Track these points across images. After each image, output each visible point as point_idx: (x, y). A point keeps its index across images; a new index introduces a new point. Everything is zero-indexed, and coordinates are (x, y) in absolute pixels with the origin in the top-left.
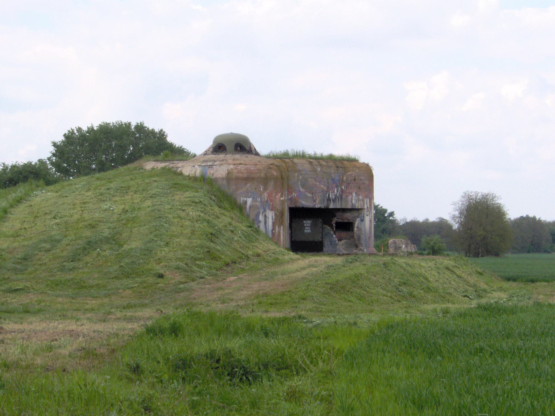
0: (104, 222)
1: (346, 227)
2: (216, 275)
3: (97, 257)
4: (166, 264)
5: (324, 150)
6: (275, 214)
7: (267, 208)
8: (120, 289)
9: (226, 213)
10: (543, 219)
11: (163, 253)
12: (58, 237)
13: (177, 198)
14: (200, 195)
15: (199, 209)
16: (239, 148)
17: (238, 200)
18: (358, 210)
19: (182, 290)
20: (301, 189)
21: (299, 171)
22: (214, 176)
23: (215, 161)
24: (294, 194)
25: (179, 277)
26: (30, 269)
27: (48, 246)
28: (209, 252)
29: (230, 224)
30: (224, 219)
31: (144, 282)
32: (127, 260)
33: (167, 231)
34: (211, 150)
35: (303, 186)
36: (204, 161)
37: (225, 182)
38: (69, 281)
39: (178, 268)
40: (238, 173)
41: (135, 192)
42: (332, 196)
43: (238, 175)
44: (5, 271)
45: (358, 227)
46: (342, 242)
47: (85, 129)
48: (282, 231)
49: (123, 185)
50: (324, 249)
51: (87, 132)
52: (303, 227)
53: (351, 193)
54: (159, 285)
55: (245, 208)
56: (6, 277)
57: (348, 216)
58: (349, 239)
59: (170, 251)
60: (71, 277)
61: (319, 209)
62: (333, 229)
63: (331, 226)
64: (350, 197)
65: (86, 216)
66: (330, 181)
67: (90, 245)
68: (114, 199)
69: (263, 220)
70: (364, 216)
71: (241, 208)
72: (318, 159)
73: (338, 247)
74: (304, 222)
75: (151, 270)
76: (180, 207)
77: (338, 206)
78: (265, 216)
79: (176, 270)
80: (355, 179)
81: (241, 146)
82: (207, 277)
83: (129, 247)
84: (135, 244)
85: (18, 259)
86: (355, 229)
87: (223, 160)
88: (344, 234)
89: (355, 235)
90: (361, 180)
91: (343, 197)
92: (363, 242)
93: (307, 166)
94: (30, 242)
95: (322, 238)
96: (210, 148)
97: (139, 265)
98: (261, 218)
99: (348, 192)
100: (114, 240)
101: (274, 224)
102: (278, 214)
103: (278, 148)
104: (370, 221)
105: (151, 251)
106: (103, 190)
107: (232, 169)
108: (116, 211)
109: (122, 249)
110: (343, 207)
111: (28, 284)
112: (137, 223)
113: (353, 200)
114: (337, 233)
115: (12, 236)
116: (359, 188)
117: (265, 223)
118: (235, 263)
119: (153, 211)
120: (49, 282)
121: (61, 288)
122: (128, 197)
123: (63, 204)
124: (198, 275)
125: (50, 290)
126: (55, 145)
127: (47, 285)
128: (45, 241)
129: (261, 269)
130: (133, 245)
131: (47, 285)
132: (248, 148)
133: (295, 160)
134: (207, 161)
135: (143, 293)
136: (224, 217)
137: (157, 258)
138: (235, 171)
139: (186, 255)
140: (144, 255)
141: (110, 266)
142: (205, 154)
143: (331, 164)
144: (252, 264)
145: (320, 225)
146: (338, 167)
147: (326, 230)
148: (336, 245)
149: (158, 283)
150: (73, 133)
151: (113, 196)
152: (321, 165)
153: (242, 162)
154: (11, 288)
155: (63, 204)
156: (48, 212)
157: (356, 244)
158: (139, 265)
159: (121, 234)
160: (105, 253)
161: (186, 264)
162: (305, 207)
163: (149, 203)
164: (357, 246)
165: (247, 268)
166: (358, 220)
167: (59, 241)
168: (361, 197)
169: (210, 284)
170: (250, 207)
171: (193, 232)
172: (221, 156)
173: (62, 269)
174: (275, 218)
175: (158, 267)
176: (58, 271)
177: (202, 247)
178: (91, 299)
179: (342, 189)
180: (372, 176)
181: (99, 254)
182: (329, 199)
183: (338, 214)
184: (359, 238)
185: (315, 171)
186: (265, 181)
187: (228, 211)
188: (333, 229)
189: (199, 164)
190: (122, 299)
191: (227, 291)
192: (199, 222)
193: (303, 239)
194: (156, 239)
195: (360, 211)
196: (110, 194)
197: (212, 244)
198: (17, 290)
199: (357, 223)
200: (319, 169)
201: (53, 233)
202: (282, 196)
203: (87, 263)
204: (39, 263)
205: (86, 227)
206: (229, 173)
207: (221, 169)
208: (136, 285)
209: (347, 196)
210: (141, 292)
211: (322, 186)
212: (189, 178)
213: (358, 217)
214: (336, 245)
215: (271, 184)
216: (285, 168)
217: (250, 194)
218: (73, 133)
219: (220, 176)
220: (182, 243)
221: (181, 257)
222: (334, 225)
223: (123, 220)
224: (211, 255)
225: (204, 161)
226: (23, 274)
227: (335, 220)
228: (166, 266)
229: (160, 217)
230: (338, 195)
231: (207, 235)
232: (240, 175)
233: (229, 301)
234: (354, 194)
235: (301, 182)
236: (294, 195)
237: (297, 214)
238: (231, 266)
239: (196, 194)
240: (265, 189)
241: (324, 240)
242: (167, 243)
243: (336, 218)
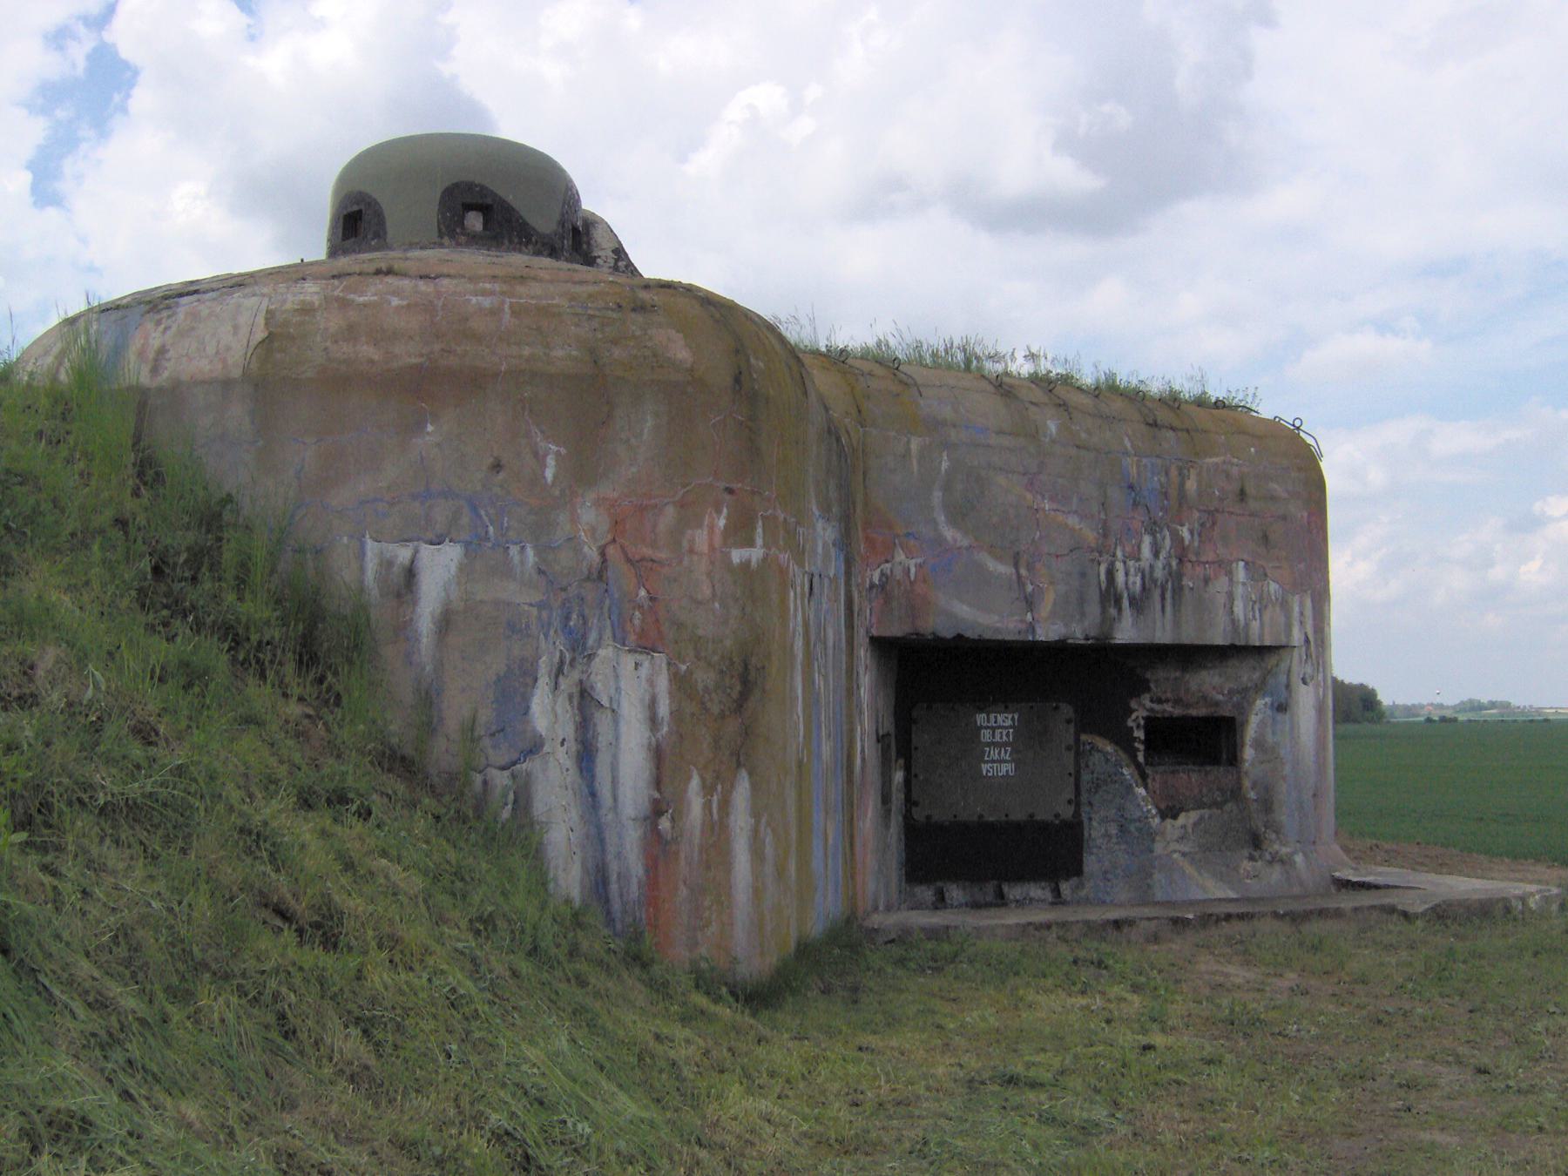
1: (1204, 741)
6: (681, 683)
18: (1262, 651)
20: (949, 533)
21: (934, 425)
24: (900, 556)
35: (959, 514)
37: (238, 414)
42: (1127, 579)
43: (345, 349)
45: (1259, 744)
46: (1182, 819)
48: (740, 820)
50: (1090, 863)
52: (971, 745)
53: (1224, 566)
55: (403, 630)
58: (1218, 805)
61: (1059, 651)
62: (1134, 758)
63: (1123, 740)
64: (1221, 584)
66: (1116, 494)
69: (567, 729)
70: (1288, 686)
72: (1054, 390)
73: (1159, 848)
74: (981, 718)
77: (1163, 634)
78: (585, 698)
80: (1242, 495)
86: (1248, 753)
88: (1189, 779)
89: (1247, 783)
90: (1273, 498)
91: (1187, 582)
92: (1283, 816)
95: (1077, 804)
98: (547, 712)
99: (1210, 556)
102: (704, 678)
104: (1320, 710)
107: (306, 310)
110: (1189, 636)
113: (1233, 604)
114: (1156, 777)
116: (1265, 537)
117: (586, 756)
132: (544, 223)
138: (333, 322)
143: (1118, 404)
145: (1067, 734)
148: (1151, 836)
162: (969, 634)
164: (1256, 842)
166: (1260, 703)
168: (1273, 587)
170: (446, 622)
174: (676, 715)
179: (1177, 539)
180: (1316, 485)
182: (1110, 596)
183: (1162, 678)
184: (1267, 805)
188: (1134, 758)
193: (971, 808)
195: (1271, 661)
200: (1052, 427)
202: (740, 531)
209: (1206, 581)
211: (1073, 521)
213: (1260, 688)
215: (640, 434)
219: (203, 366)
222: (1140, 734)
227: (1140, 710)
230: (1159, 573)
232: (367, 351)
234: (1240, 573)
235: (947, 488)
236: (904, 562)
237: (933, 676)
240: (582, 472)
241: (1085, 809)
243: (1146, 699)
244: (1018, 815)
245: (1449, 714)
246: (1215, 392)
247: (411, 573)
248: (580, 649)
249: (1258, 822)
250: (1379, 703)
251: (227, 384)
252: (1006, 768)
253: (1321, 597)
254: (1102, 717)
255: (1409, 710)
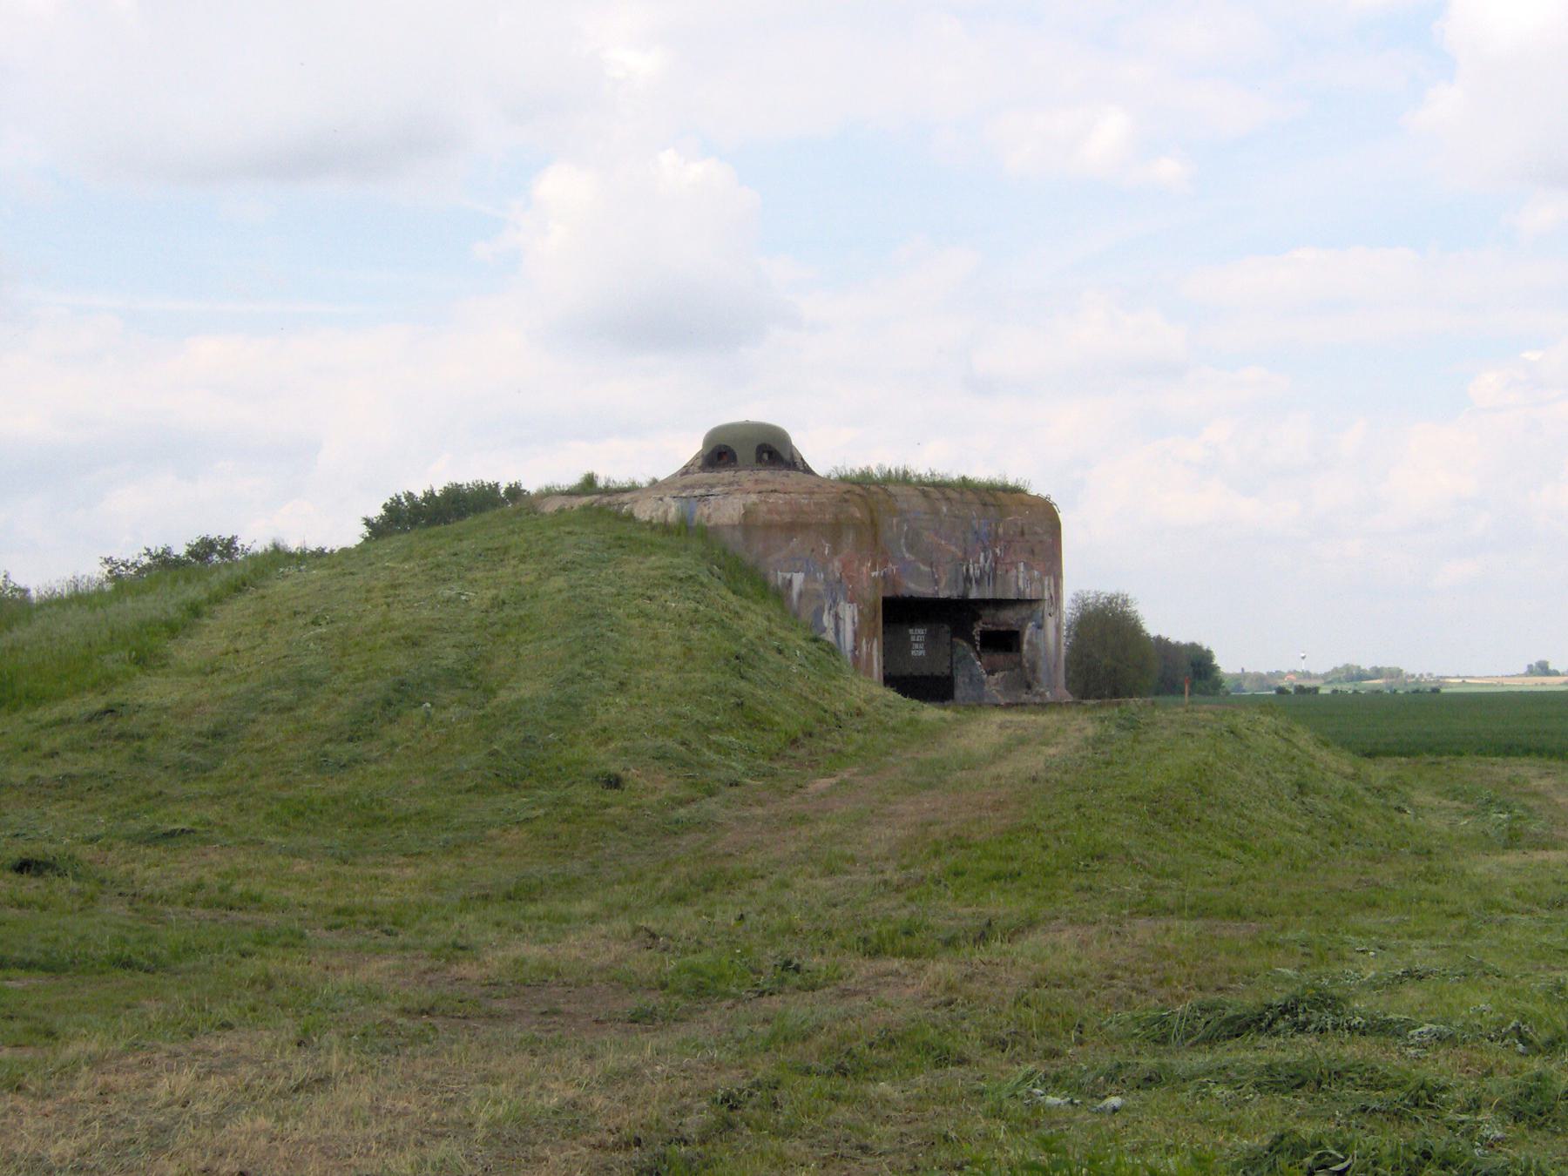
0: (443, 630)
1: (1004, 642)
2: (773, 774)
3: (423, 727)
4: (627, 744)
5: (951, 470)
6: (860, 612)
7: (840, 597)
8: (490, 825)
9: (753, 607)
10: (1173, 639)
11: (613, 711)
12: (317, 674)
13: (628, 569)
14: (685, 563)
15: (691, 595)
16: (766, 456)
17: (771, 578)
18: (1030, 602)
19: (684, 827)
22: (712, 523)
23: (712, 486)
25: (668, 786)
26: (229, 766)
27: (287, 696)
28: (740, 705)
29: (770, 633)
30: (755, 620)
31: (566, 802)
32: (508, 736)
33: (616, 650)
34: (700, 462)
35: (910, 548)
36: (685, 487)
37: (738, 536)
38: (336, 801)
39: (661, 756)
40: (770, 511)
41: (523, 559)
42: (974, 571)
44: (155, 771)
45: (1029, 643)
47: (419, 494)
48: (875, 653)
49: (490, 545)
50: (958, 694)
51: (424, 500)
52: (908, 645)
53: (1014, 564)
54: (611, 811)
55: (789, 598)
56: (153, 790)
57: (1008, 617)
59: (631, 706)
60: (343, 787)
63: (970, 640)
65: (397, 616)
66: (970, 536)
67: (403, 693)
68: (470, 576)
71: (780, 595)
73: (986, 688)
75: (583, 763)
76: (640, 590)
77: (988, 595)
78: (837, 617)
79: (657, 763)
80: (1022, 533)
81: (771, 451)
82: (748, 781)
83: (514, 696)
84: (528, 688)
85: (199, 734)
86: (1025, 647)
87: (731, 484)
88: (1000, 658)
92: (1041, 675)
93: (918, 502)
94: (244, 686)
96: (696, 458)
97: (545, 749)
98: (827, 620)
100: (469, 678)
101: (856, 635)
102: (866, 611)
103: (854, 463)
105: (576, 706)
106: (442, 556)
108: (473, 604)
109: (495, 702)
110: (999, 596)
111: (212, 813)
112: (533, 632)
113: (1019, 581)
114: (985, 658)
115: (201, 672)
118: (810, 735)
119: (570, 600)
120: (276, 807)
121: (310, 825)
122: (505, 571)
123: (342, 589)
124: (723, 774)
125: (276, 833)
126: (368, 522)
127: (270, 816)
128: (281, 684)
129: (887, 753)
130: (526, 690)
131: (270, 816)
132: (787, 457)
133: (891, 488)
134: (692, 487)
135: (564, 838)
136: (750, 616)
137: (597, 725)
138: (764, 508)
139: (680, 716)
140: (559, 717)
141: (461, 753)
142: (686, 471)
143: (970, 496)
144: (859, 737)
146: (985, 505)
147: (960, 652)
148: (982, 682)
149: (607, 806)
150: (398, 501)
151: (470, 569)
152: (948, 499)
153: (778, 487)
154: (154, 827)
155: (342, 589)
156: (301, 609)
157: (1025, 680)
158: (545, 749)
159: (489, 662)
160: (444, 715)
161: (683, 743)
163: (559, 582)
164: (1029, 687)
165: (851, 749)
167: (317, 683)
169: (760, 803)
170: (800, 595)
171: (688, 653)
172: (726, 475)
173: (320, 765)
175: (601, 755)
176: (306, 770)
177: (720, 692)
178: (402, 860)
179: (995, 554)
181: (428, 718)
182: (967, 579)
183: (987, 613)
184: (1034, 670)
185: (936, 512)
186: (835, 531)
187: (756, 603)
189: (675, 493)
190: (499, 861)
191: (823, 828)
192: (698, 627)
193: (908, 670)
194: (589, 672)
195: (1035, 606)
196: (459, 564)
197: (743, 683)
198: (172, 834)
199: (1027, 633)
201: (308, 661)
202: (873, 568)
203: (394, 744)
204: (257, 745)
205: (395, 643)
206: (748, 512)
207: (726, 507)
208: (541, 812)
210: (556, 837)
211: (953, 548)
212: (651, 526)
213: (1030, 618)
214: (982, 682)
215: (850, 537)
216: (871, 503)
217: (798, 564)
218: (398, 501)
219: (725, 520)
220: (665, 684)
221: (668, 721)
223: (493, 624)
224: (750, 717)
225: (685, 487)
226: (205, 780)
227: (978, 628)
228: (626, 751)
229: (592, 616)
230: (987, 568)
231: (727, 662)
232: (777, 518)
233: (847, 866)
236: (892, 568)
237: (899, 612)
238: (803, 746)
239: (676, 561)
240: (835, 551)
242: (621, 684)
244: (926, 673)
245: (1307, 684)
246: (1011, 482)
247: (790, 581)
248: (835, 602)
249: (1030, 678)
250: (1215, 669)
251: (734, 526)
252: (922, 653)
253: (1058, 577)
254: (962, 631)
255: (1259, 678)
